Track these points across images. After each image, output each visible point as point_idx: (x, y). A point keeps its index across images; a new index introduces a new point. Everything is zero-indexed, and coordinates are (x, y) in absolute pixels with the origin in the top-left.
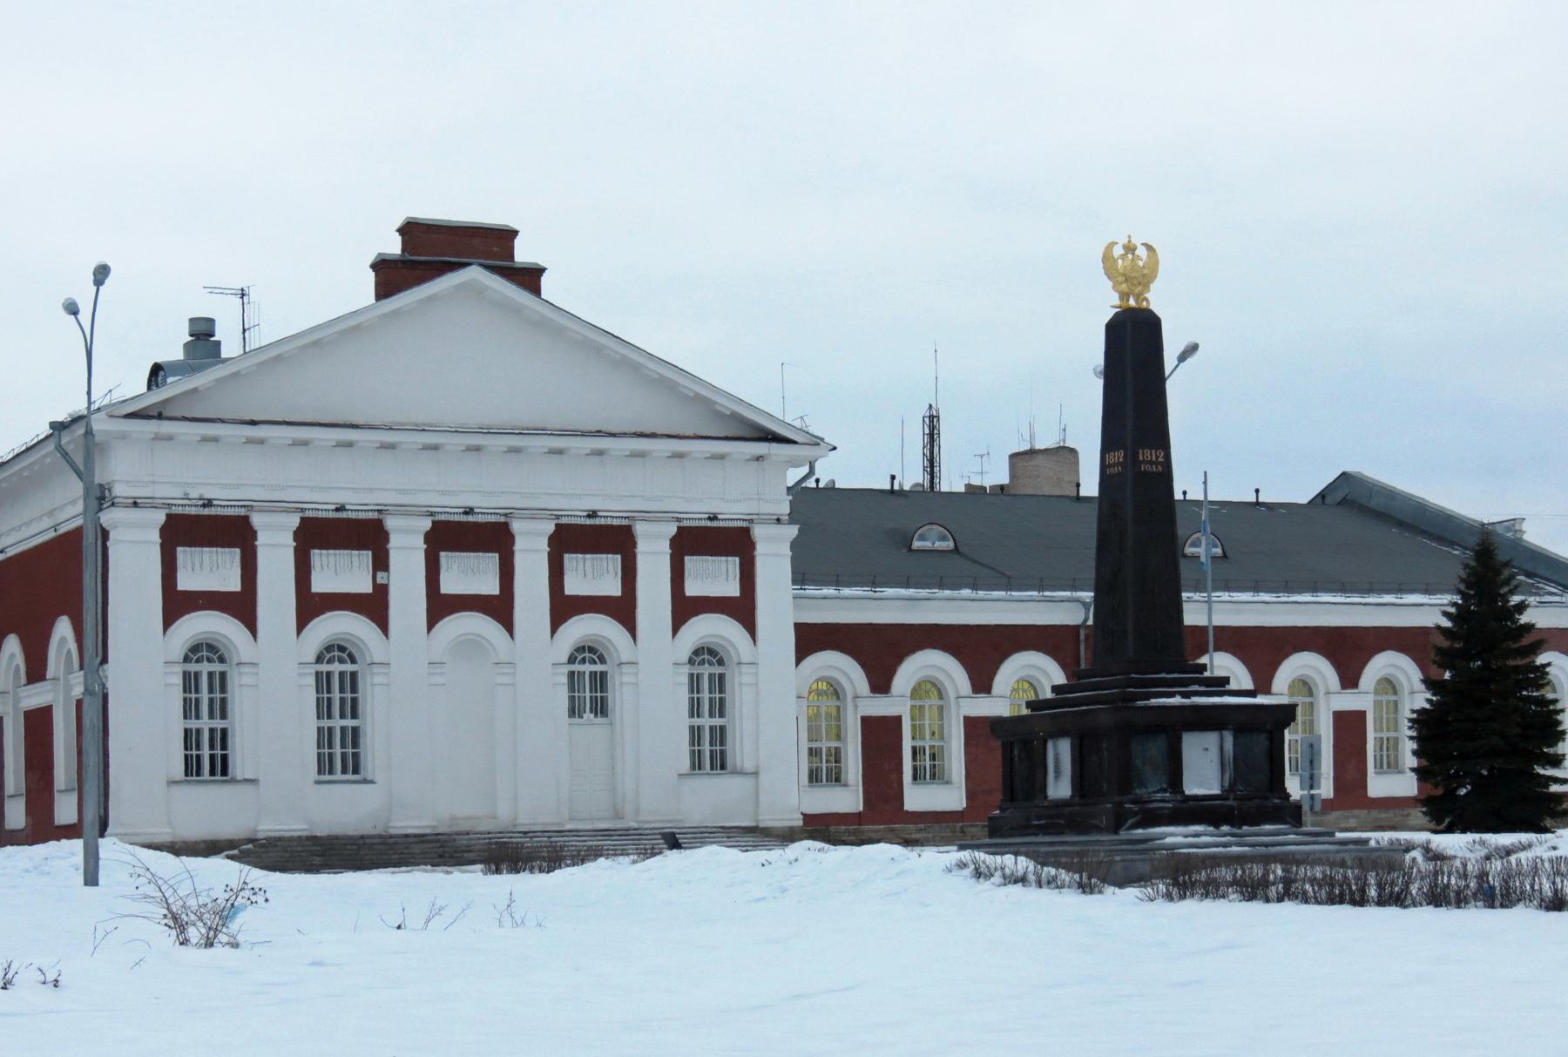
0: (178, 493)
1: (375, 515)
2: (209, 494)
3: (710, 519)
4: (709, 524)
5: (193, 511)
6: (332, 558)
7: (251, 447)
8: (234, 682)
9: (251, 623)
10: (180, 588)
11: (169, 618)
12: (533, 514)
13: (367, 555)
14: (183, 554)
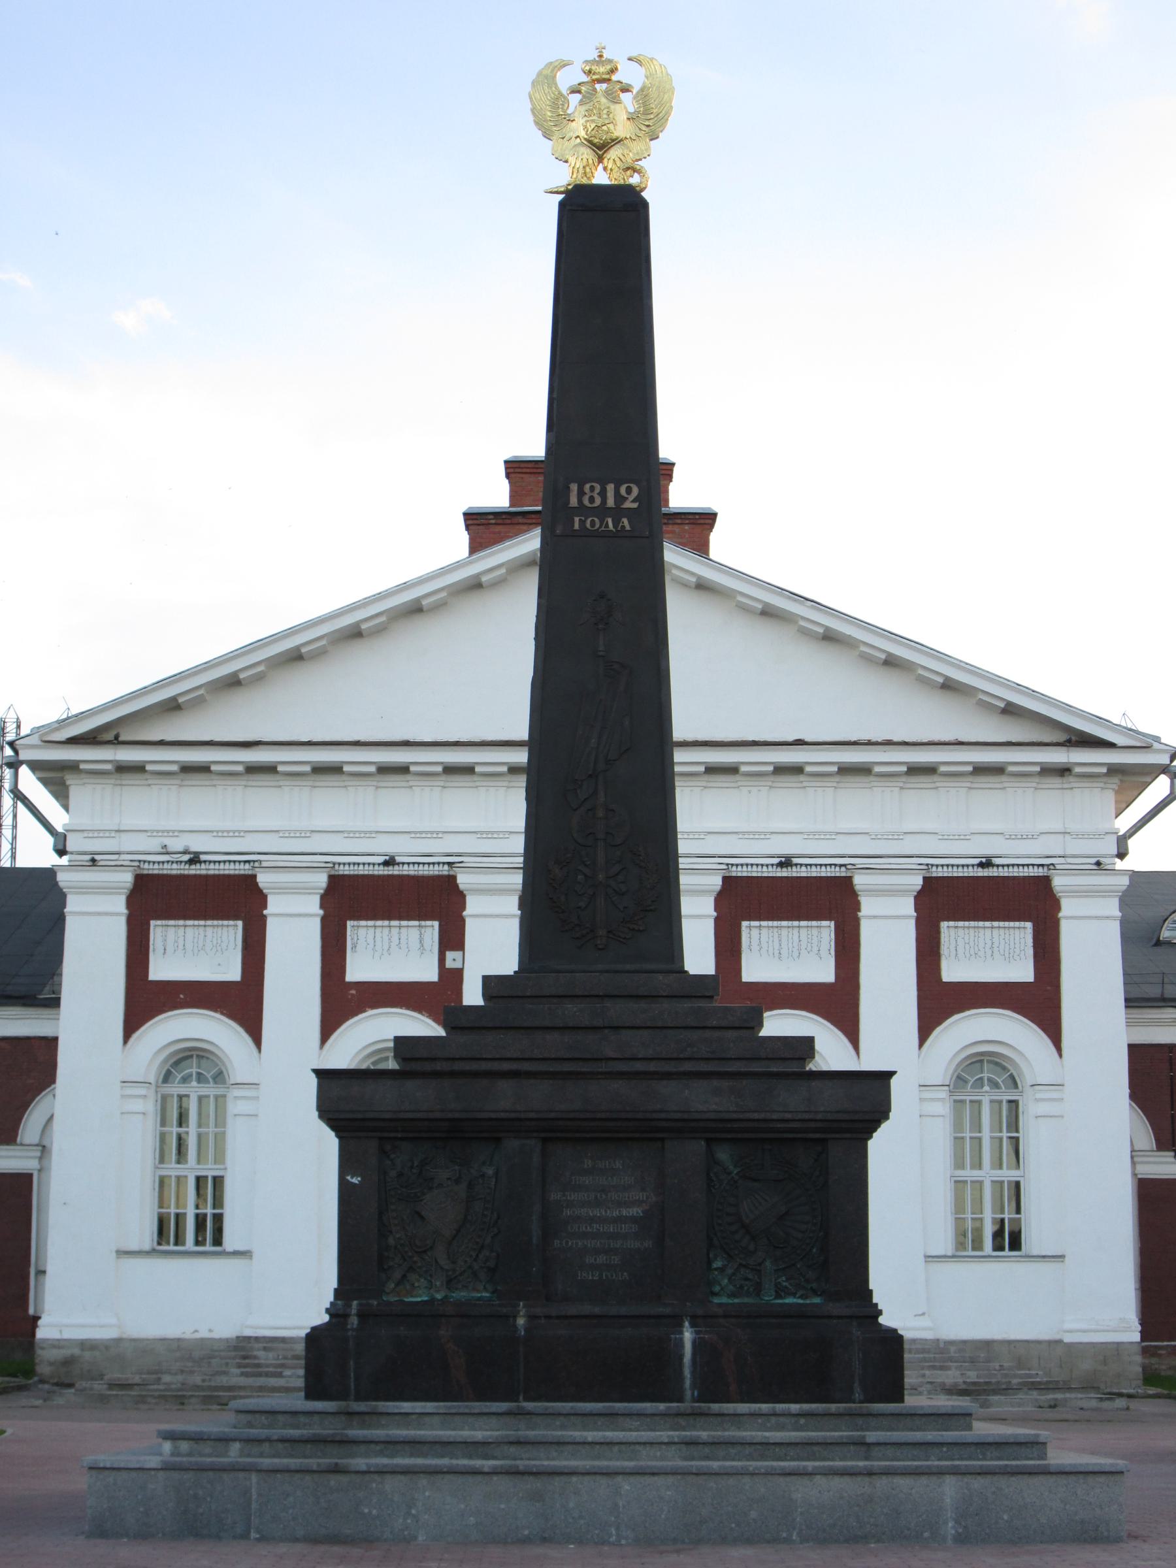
0: (154, 844)
1: (445, 870)
2: (197, 844)
3: (981, 865)
4: (981, 872)
5: (175, 870)
6: (395, 931)
7: (982, 781)
8: (1031, 1109)
9: (253, 1026)
10: (744, 980)
11: (134, 1021)
12: (292, 861)
13: (431, 930)
14: (948, 929)
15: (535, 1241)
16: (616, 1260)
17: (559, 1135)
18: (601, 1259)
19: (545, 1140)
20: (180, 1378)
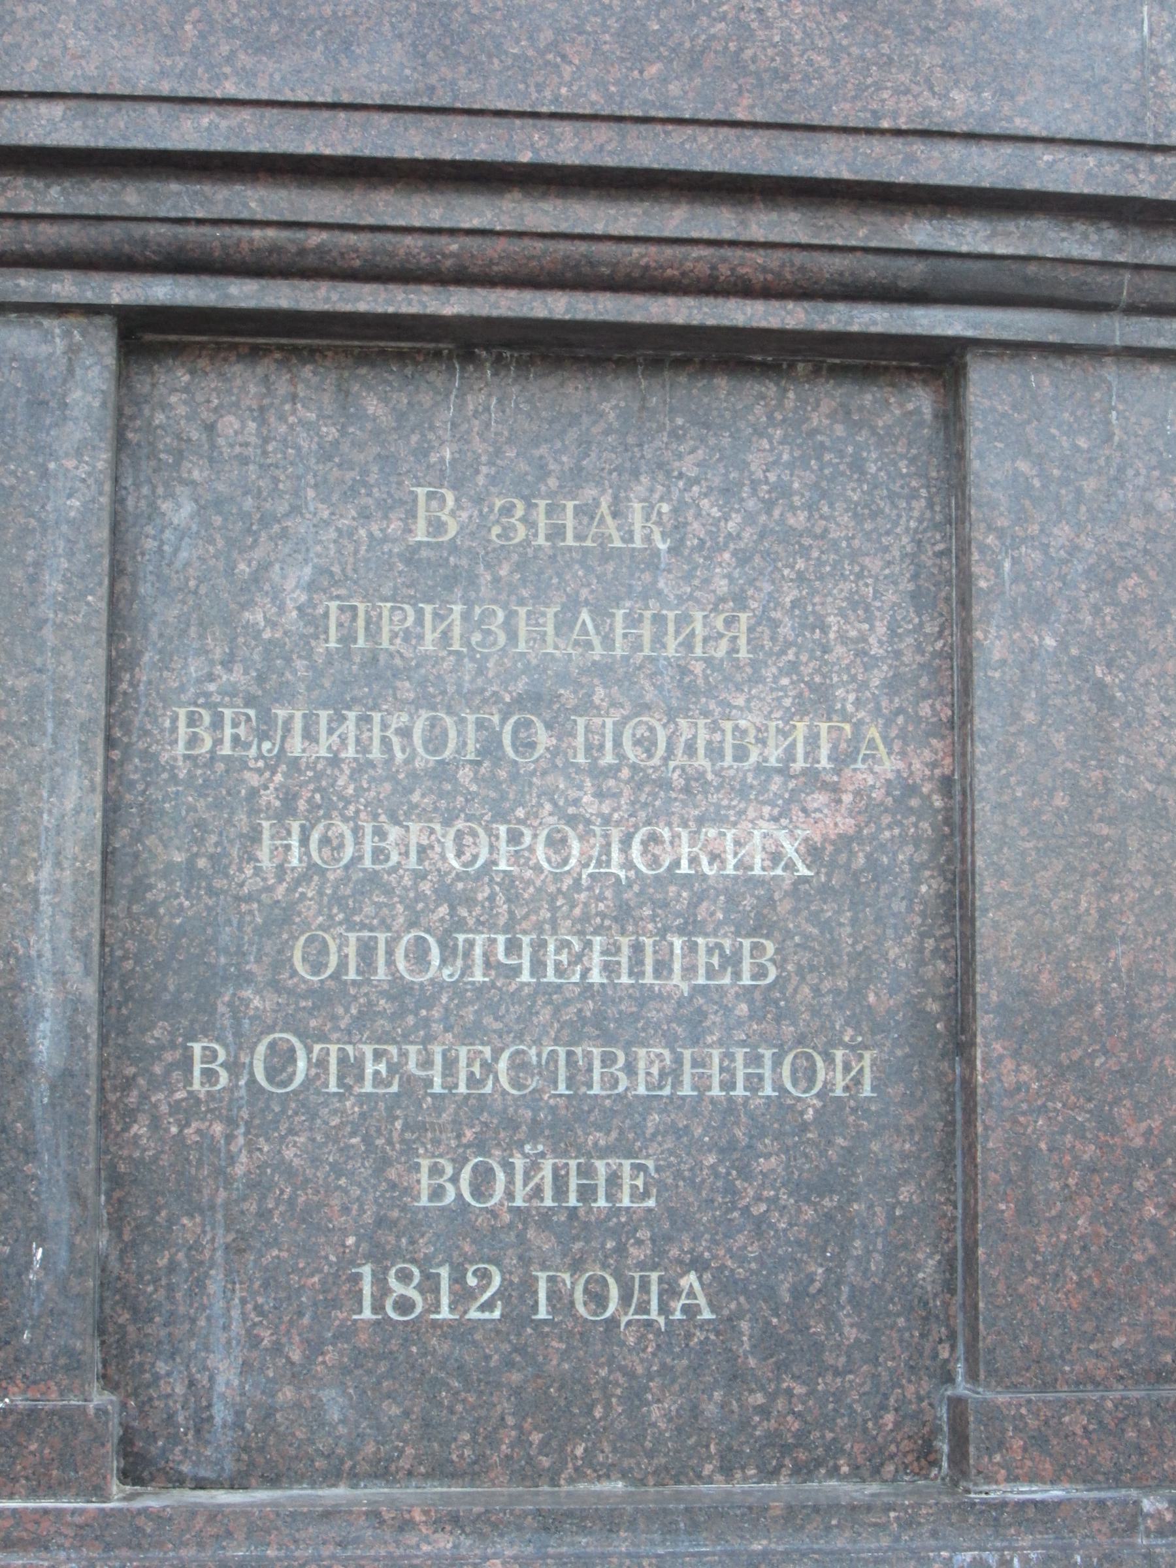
15: (45, 1043)
16: (626, 1186)
17: (242, 294)
18: (523, 1180)
19: (145, 337)
20: (681, 1549)
